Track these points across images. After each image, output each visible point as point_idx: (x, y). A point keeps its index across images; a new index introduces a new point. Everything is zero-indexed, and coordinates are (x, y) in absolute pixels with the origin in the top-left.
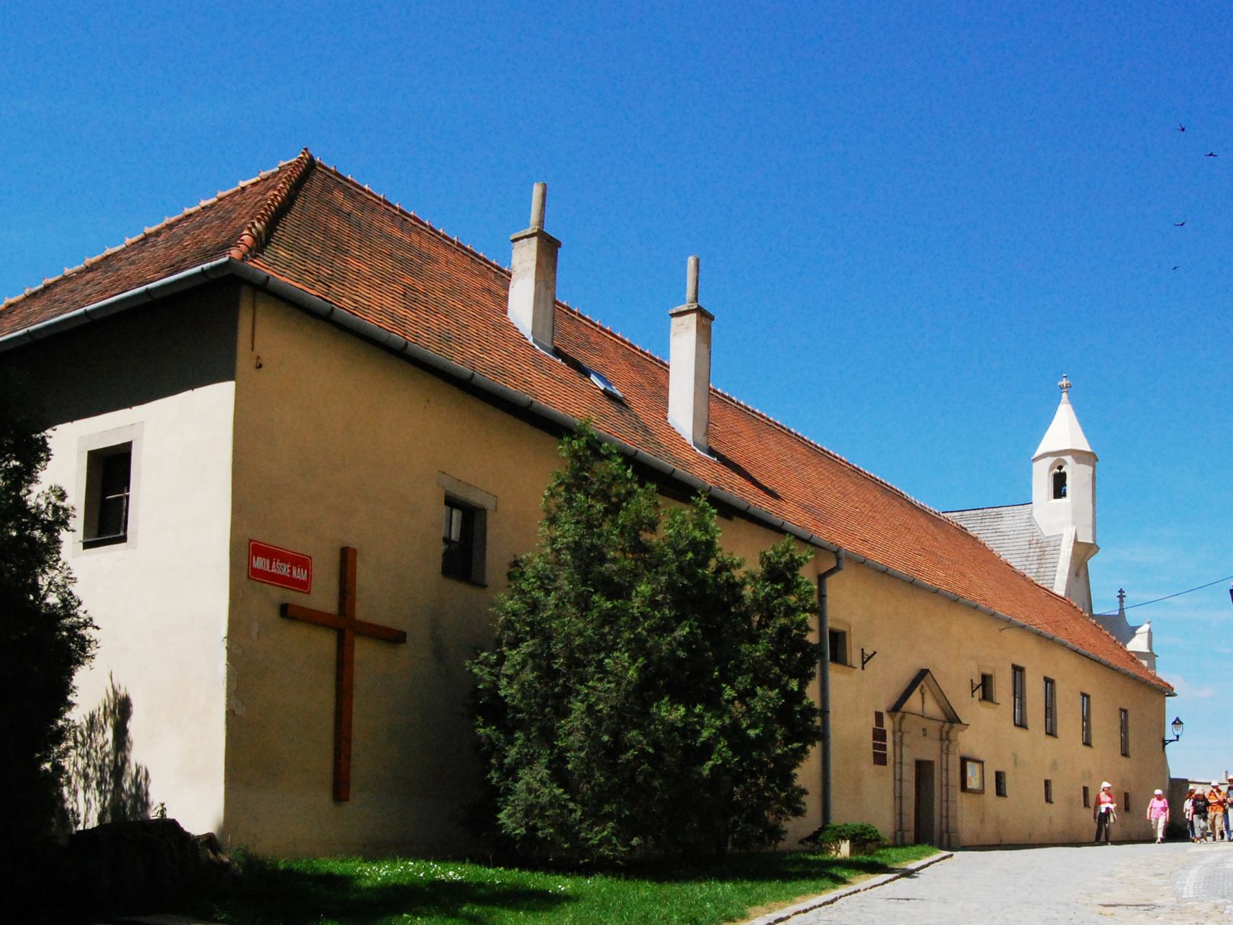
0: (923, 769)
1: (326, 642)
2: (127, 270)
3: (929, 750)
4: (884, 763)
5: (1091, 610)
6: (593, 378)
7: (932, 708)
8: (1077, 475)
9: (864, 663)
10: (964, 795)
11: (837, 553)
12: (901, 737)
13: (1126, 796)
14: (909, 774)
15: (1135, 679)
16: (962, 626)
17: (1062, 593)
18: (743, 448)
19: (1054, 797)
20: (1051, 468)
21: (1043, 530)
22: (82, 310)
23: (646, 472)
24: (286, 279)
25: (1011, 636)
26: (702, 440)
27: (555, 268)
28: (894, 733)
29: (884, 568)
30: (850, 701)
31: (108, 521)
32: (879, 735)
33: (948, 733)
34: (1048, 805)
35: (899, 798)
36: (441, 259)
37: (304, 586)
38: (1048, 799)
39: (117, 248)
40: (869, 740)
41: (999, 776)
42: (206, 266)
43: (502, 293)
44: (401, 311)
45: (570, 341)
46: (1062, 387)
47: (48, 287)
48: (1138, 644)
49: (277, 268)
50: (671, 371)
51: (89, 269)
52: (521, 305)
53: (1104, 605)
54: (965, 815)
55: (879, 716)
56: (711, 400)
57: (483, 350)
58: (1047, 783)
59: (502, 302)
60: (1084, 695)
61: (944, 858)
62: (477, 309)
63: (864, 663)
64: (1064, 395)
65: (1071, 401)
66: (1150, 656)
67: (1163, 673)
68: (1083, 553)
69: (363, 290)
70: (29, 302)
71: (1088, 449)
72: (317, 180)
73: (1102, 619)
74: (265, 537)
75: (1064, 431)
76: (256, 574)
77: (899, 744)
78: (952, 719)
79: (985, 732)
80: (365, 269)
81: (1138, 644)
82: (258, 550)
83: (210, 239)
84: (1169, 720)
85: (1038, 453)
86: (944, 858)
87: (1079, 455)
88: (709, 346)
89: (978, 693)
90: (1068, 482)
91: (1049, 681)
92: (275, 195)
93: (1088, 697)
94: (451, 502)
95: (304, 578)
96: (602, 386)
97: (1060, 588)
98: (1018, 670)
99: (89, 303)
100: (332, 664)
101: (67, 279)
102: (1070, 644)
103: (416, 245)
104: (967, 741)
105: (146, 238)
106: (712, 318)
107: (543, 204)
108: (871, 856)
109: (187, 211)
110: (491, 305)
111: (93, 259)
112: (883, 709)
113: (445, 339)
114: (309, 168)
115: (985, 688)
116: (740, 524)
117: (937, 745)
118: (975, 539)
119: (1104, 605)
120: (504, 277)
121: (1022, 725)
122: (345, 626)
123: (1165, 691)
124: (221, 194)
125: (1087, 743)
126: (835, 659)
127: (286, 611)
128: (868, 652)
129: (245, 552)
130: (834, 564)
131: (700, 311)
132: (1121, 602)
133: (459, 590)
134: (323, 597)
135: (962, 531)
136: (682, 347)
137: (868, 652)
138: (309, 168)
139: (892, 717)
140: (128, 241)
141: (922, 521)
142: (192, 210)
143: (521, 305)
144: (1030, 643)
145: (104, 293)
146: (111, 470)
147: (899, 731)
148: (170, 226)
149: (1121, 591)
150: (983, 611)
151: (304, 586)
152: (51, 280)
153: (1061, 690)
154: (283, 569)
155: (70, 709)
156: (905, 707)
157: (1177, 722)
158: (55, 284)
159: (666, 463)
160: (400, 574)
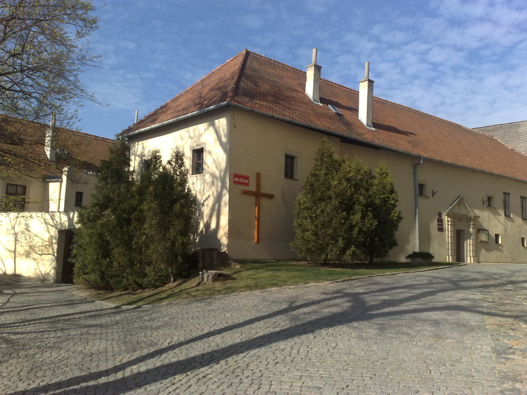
9: (433, 195)
11: (419, 158)
37: (247, 184)
59: (303, 86)
61: (121, 295)
63: (433, 195)
72: (250, 57)
76: (236, 182)
82: (236, 176)
86: (121, 295)
89: (486, 204)
95: (247, 182)
122: (258, 195)
128: (434, 191)
133: (289, 181)
134: (252, 187)
138: (248, 53)
151: (247, 184)
154: (242, 180)
155: (160, 157)
160: (273, 179)
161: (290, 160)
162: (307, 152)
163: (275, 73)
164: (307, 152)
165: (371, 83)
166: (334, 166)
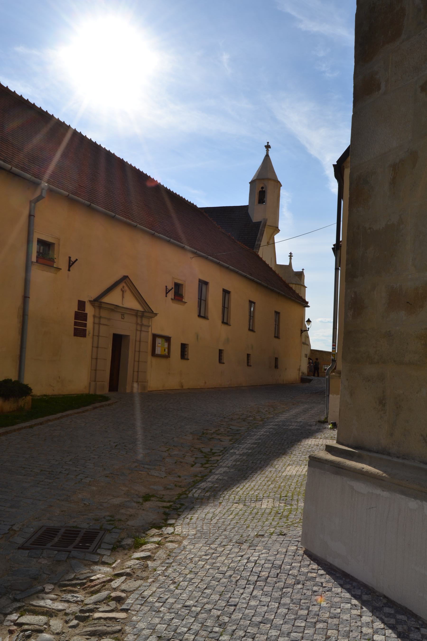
0: (118, 341)
10: (155, 360)
19: (225, 360)
38: (220, 361)
41: (184, 347)
55: (81, 304)
89: (171, 295)
91: (226, 292)
94: (251, 366)
98: (203, 284)
108: (385, 597)
112: (85, 299)
115: (178, 292)
128: (73, 259)
132: (291, 259)
137: (73, 259)
149: (291, 253)
153: (233, 297)
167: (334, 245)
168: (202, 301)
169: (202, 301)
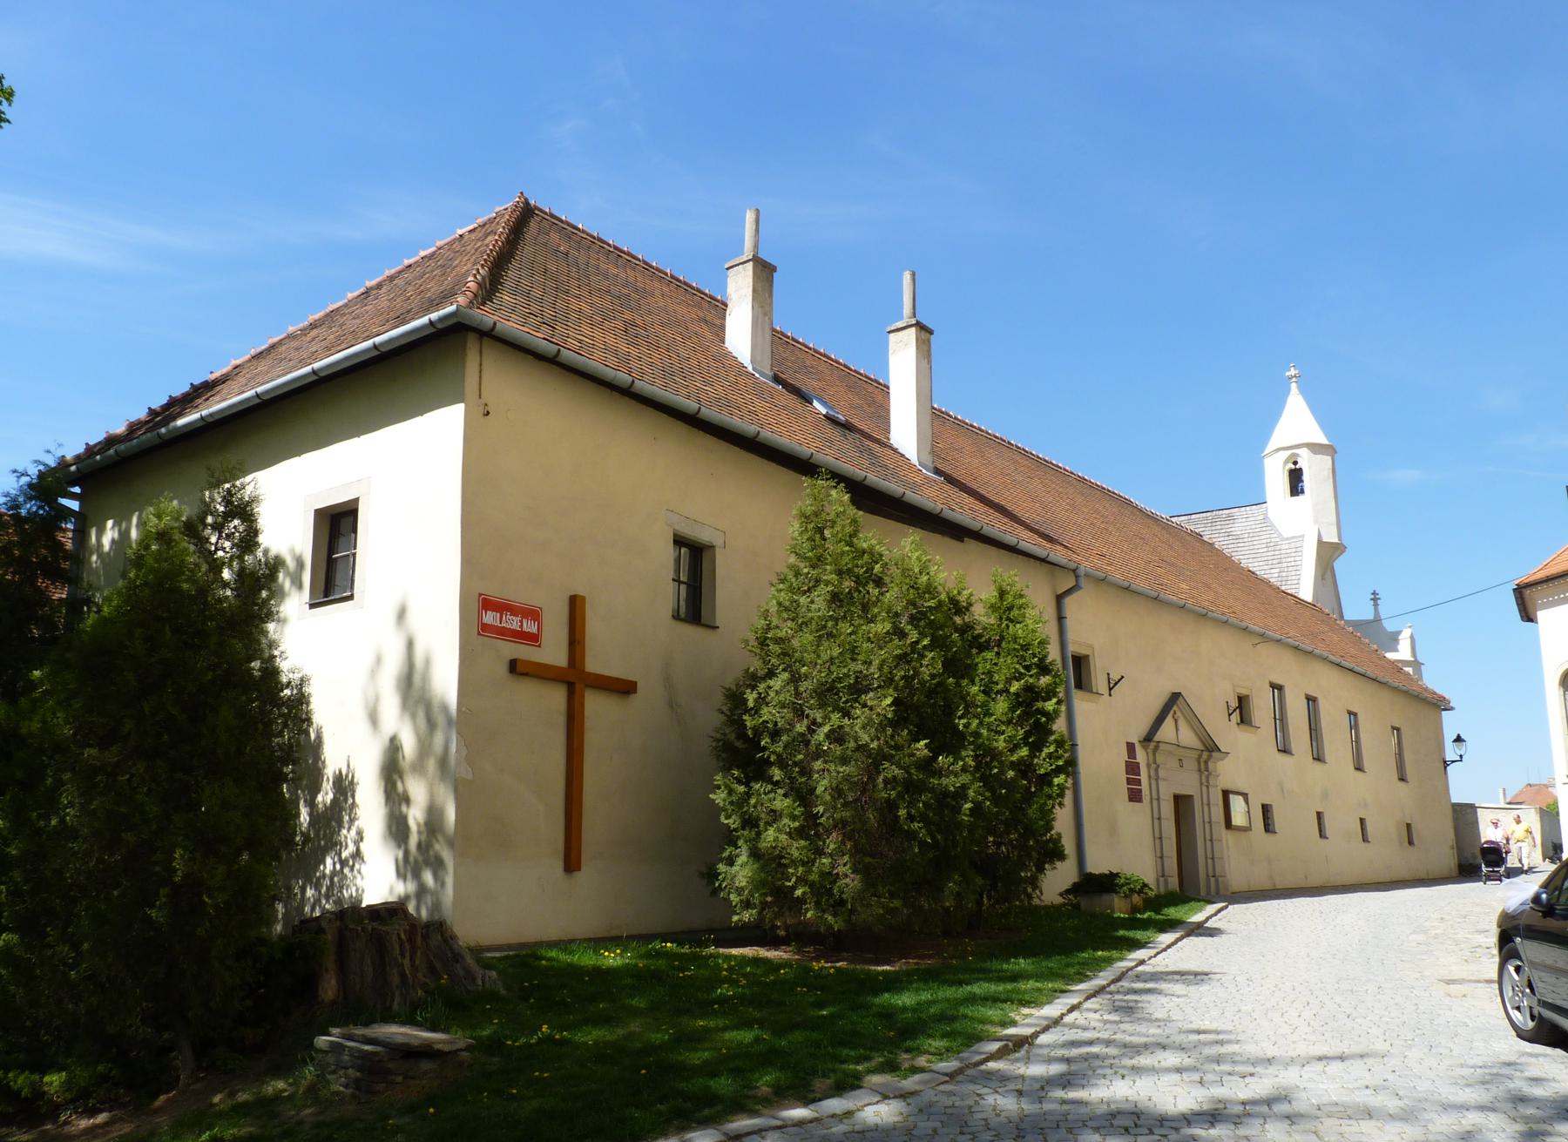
0: (1182, 803)
1: (557, 697)
2: (351, 324)
3: (1187, 783)
4: (1140, 800)
5: (1342, 617)
6: (816, 403)
7: (1187, 737)
8: (1315, 469)
10: (1229, 832)
12: (1156, 770)
13: (1408, 826)
14: (1168, 809)
15: (1407, 694)
16: (1210, 641)
17: (1310, 599)
18: (968, 466)
20: (1286, 462)
21: (1284, 536)
22: (308, 369)
23: (869, 498)
24: (511, 325)
25: (1265, 650)
26: (928, 460)
27: (771, 295)
28: (1148, 766)
29: (1126, 584)
30: (1100, 730)
31: (332, 578)
32: (1132, 768)
33: (1206, 762)
34: (1270, 837)
35: (1159, 838)
36: (657, 293)
39: (340, 304)
40: (1123, 776)
41: (1266, 809)
42: (434, 316)
43: (718, 322)
44: (623, 348)
45: (792, 368)
46: (1291, 378)
47: (273, 347)
48: (1403, 653)
49: (504, 316)
50: (892, 391)
51: (313, 326)
52: (739, 336)
53: (1356, 609)
54: (1236, 859)
55: (1131, 748)
56: (936, 421)
57: (706, 383)
58: (1319, 815)
60: (1350, 713)
61: (1219, 911)
62: (695, 339)
64: (1294, 386)
65: (1302, 391)
66: (1416, 664)
67: (1433, 680)
68: (1328, 554)
69: (586, 329)
70: (254, 362)
71: (1324, 441)
72: (533, 225)
73: (1357, 624)
74: (495, 591)
75: (1297, 423)
76: (485, 628)
77: (1155, 778)
78: (1211, 747)
79: (1247, 760)
80: (586, 308)
81: (1403, 653)
82: (487, 604)
83: (434, 289)
84: (1449, 736)
85: (1270, 447)
87: (1315, 448)
88: (929, 362)
89: (1236, 717)
90: (1306, 477)
91: (1311, 700)
92: (493, 242)
93: (1355, 715)
94: (679, 541)
95: (534, 630)
96: (824, 411)
97: (1306, 594)
99: (316, 360)
100: (561, 720)
101: (291, 337)
102: (1331, 658)
103: (631, 279)
104: (1228, 772)
105: (367, 293)
106: (931, 332)
107: (757, 230)
109: (406, 262)
110: (709, 335)
111: (317, 316)
112: (1135, 740)
113: (667, 373)
114: (526, 214)
116: (971, 545)
117: (1196, 776)
118: (1212, 545)
119: (1356, 609)
120: (721, 307)
121: (1285, 750)
122: (574, 679)
123: (1439, 704)
124: (439, 243)
125: (1359, 768)
126: (1079, 686)
127: (514, 667)
129: (474, 606)
130: (1071, 583)
131: (920, 326)
132: (1376, 605)
134: (553, 652)
135: (1198, 537)
136: (901, 366)
137: (1115, 677)
138: (526, 214)
139: (1145, 748)
140: (350, 296)
141: (1156, 529)
142: (411, 261)
143: (739, 336)
144: (1288, 658)
145: (329, 350)
146: (337, 525)
147: (1154, 766)
148: (391, 278)
150: (1216, 621)
151: (533, 639)
152: (276, 339)
153: (1323, 706)
154: (513, 623)
156: (1157, 738)
157: (1459, 739)
158: (280, 342)
159: (893, 487)
160: (632, 624)
161: (695, 558)
162: (758, 531)
163: (623, 275)
164: (758, 531)
165: (924, 335)
166: (857, 586)
167: (152, 412)
168: (1281, 720)
169: (1281, 720)
